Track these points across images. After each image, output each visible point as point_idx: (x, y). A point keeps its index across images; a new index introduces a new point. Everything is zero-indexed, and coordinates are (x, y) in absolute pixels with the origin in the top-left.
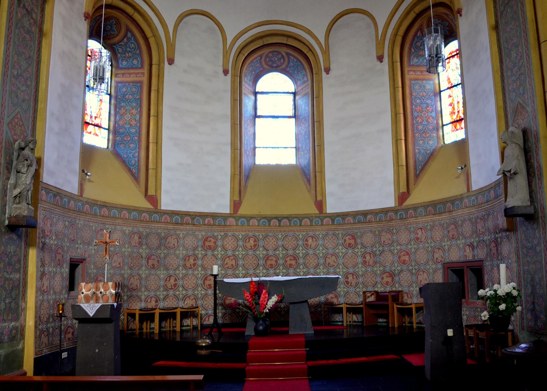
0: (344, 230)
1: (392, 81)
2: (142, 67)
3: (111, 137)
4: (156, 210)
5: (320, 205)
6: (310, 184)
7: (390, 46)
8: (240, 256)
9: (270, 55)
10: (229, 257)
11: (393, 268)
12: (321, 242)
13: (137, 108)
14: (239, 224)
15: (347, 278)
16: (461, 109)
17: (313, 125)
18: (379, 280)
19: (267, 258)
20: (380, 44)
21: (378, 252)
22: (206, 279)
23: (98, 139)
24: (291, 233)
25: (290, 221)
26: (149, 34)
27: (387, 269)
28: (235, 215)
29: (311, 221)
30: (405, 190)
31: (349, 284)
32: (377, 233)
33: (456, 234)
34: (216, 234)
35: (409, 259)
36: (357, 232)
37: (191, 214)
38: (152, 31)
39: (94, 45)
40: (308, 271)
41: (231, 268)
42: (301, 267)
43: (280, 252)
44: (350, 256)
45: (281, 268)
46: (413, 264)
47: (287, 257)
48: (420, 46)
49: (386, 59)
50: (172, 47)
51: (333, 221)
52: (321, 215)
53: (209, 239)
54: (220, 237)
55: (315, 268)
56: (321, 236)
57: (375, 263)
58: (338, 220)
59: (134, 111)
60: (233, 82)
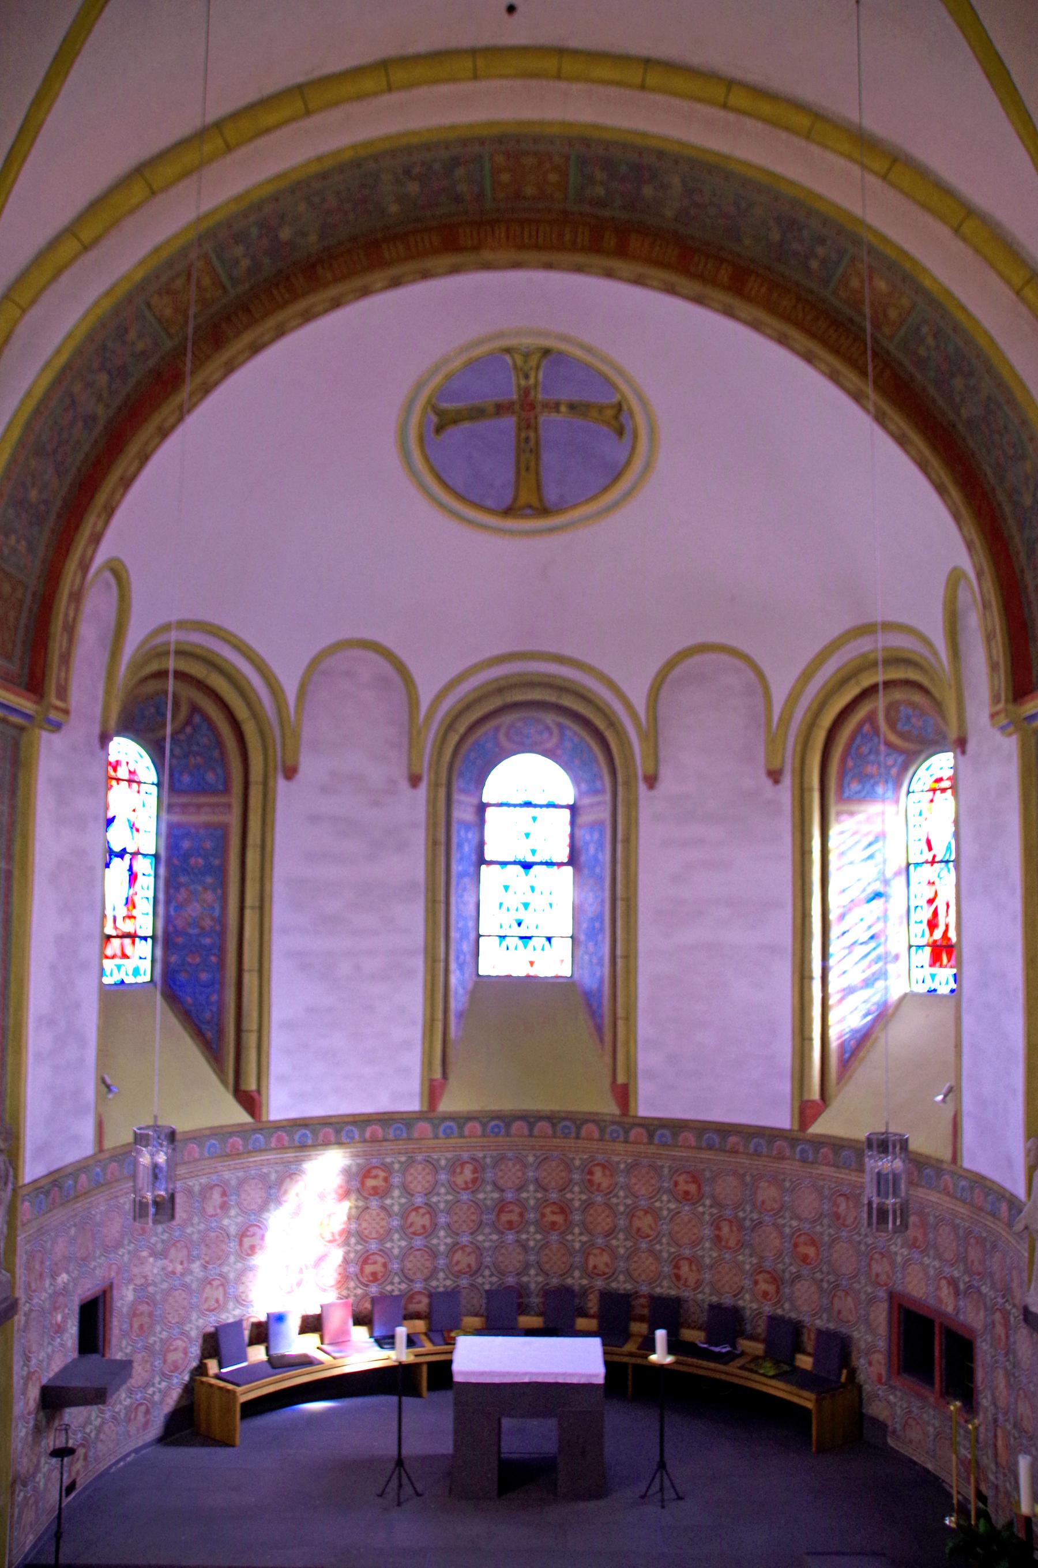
0: (674, 1159)
1: (798, 835)
2: (227, 790)
3: (159, 953)
4: (260, 1125)
5: (623, 1094)
6: (602, 1040)
7: (799, 748)
8: (442, 1206)
9: (519, 724)
10: (417, 1209)
11: (780, 1266)
12: (622, 1180)
13: (214, 890)
14: (441, 1135)
15: (677, 1267)
16: (952, 920)
17: (607, 858)
18: (747, 1283)
19: (501, 1207)
20: (774, 740)
21: (748, 1223)
22: (366, 1261)
23: (136, 965)
24: (555, 1154)
25: (554, 1125)
26: (242, 712)
27: (768, 1265)
28: (432, 1115)
29: (602, 1131)
30: (815, 1095)
31: (682, 1282)
32: (748, 1178)
33: (920, 1238)
34: (388, 1160)
35: (817, 1254)
36: (704, 1170)
37: (333, 1120)
38: (249, 705)
39: (125, 750)
40: (590, 1198)
41: (419, 1235)
42: (577, 1230)
43: (531, 1195)
44: (686, 1219)
45: (532, 1229)
46: (825, 1268)
47: (545, 1207)
48: (870, 752)
49: (787, 780)
50: (291, 734)
51: (651, 1136)
52: (626, 1120)
53: (374, 1172)
54: (397, 1166)
55: (607, 1236)
56: (622, 1166)
57: (742, 1245)
58: (663, 1135)
59: (209, 896)
60: (432, 802)
